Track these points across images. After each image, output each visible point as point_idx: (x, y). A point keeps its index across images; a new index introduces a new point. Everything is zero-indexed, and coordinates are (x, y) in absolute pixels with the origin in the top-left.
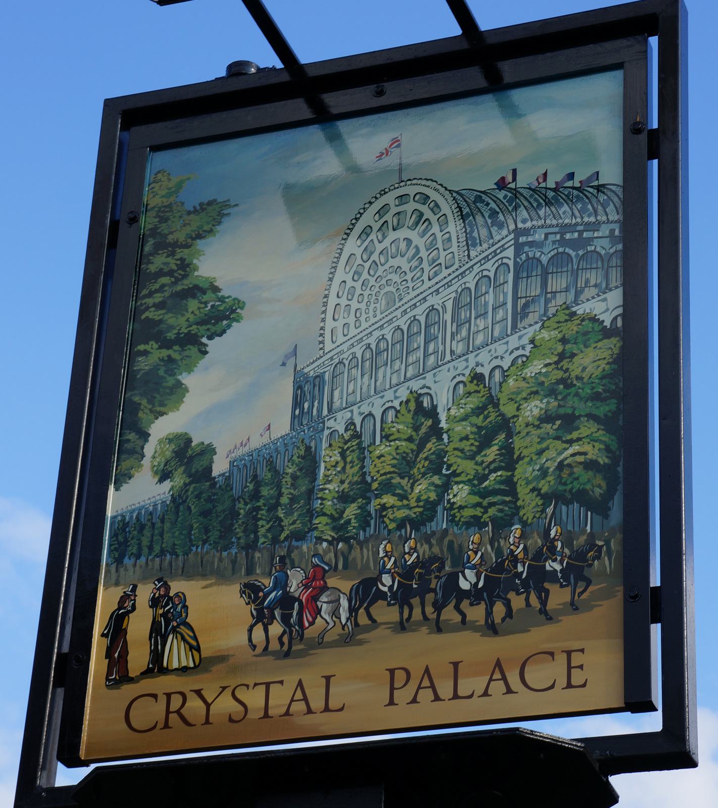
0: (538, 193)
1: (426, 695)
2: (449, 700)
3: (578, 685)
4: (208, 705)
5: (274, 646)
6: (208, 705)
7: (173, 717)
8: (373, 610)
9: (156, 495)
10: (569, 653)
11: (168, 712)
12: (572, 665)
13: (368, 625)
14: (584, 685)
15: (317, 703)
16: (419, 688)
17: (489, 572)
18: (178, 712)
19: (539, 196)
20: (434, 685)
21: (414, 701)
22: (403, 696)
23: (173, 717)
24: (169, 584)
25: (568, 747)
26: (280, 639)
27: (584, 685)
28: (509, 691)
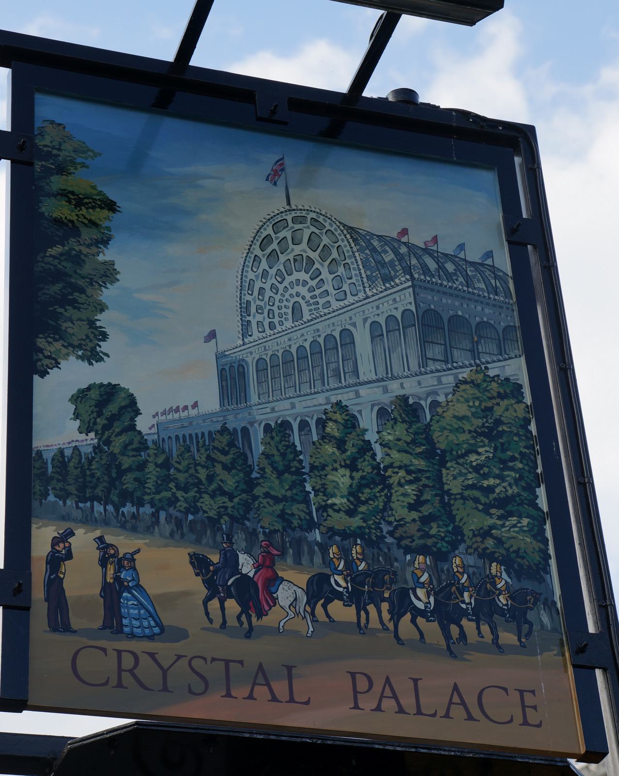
0: (482, 273)
1: (389, 704)
2: (286, 702)
3: (99, 683)
4: (165, 672)
5: (232, 622)
6: (165, 672)
7: (126, 676)
8: (330, 607)
9: (42, 445)
10: (521, 692)
11: (120, 670)
12: (384, 695)
13: (236, 627)
14: (539, 726)
15: (408, 702)
16: (382, 697)
17: (483, 597)
18: (131, 671)
19: (482, 276)
20: (465, 702)
21: (378, 708)
22: (368, 703)
23: (127, 678)
24: (74, 532)
25: (313, 743)
26: (239, 617)
27: (539, 726)
28: (470, 718)
